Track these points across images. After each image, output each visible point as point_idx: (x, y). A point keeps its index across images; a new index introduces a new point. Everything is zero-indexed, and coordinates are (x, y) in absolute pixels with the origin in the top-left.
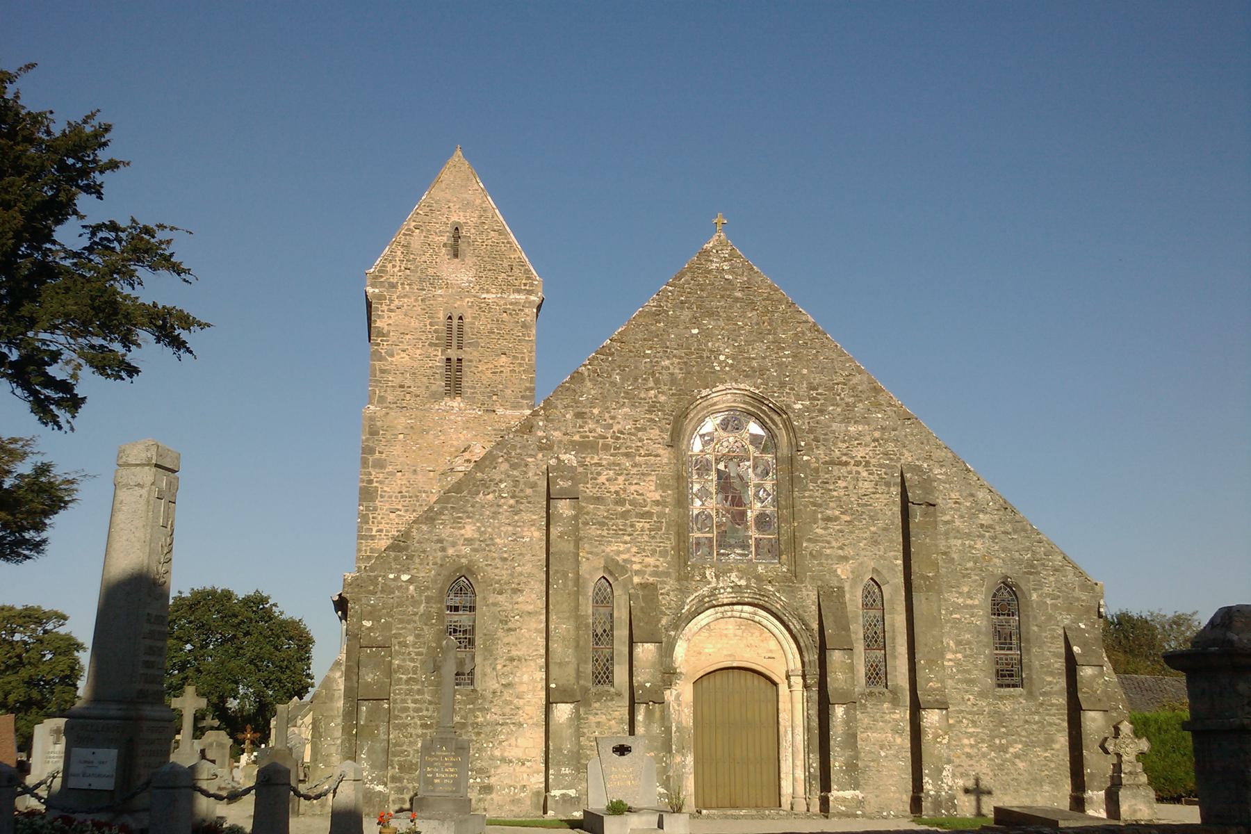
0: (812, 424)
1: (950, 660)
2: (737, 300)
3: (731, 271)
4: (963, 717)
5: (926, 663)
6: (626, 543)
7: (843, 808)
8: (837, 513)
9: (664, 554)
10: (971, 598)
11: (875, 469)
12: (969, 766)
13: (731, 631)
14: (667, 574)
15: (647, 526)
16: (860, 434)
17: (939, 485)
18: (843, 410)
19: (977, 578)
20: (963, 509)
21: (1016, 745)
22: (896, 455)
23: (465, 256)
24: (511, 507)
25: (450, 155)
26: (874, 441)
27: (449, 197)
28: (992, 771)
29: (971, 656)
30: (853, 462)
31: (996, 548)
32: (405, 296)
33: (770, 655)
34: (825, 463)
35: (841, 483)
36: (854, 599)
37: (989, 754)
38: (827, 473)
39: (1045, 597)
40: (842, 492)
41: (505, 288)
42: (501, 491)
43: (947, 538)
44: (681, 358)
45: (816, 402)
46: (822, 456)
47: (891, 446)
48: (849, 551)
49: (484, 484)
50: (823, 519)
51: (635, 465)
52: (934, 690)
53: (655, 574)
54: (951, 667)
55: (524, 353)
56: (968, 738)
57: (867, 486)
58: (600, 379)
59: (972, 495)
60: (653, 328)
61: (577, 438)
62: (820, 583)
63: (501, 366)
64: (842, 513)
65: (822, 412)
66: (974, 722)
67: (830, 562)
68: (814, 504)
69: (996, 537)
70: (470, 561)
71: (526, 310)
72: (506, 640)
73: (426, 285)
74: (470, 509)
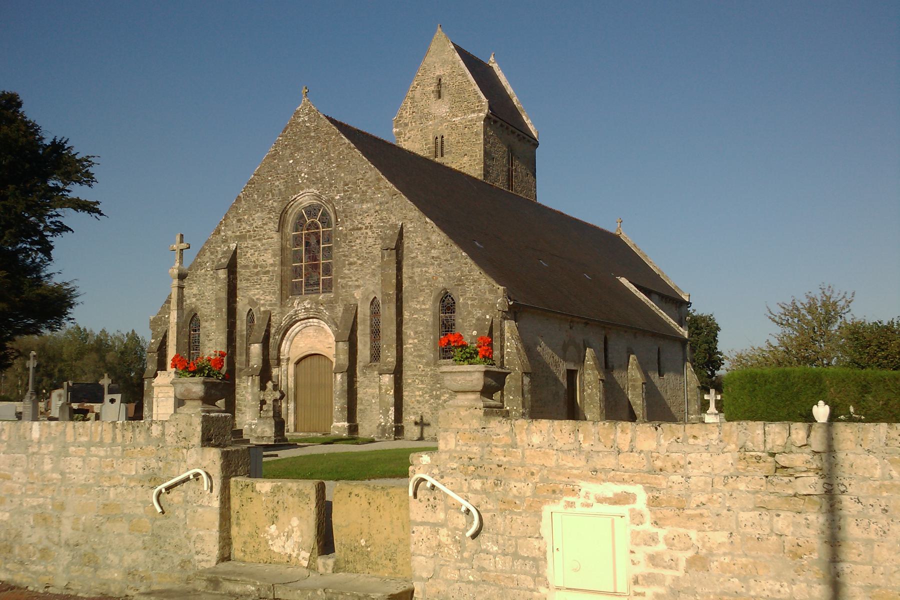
0: (344, 207)
1: (411, 344)
2: (311, 138)
3: (309, 121)
4: (416, 379)
5: (386, 347)
6: (257, 289)
7: (337, 432)
8: (355, 259)
9: (274, 293)
10: (424, 304)
11: (375, 230)
12: (419, 408)
13: (312, 334)
14: (275, 304)
15: (267, 278)
16: (369, 209)
17: (410, 235)
18: (361, 196)
19: (428, 291)
20: (423, 248)
21: (445, 395)
22: (386, 219)
23: (444, 96)
24: (211, 275)
25: (435, 31)
26: (376, 212)
27: (434, 60)
28: (431, 411)
29: (423, 341)
30: (364, 227)
31: (441, 271)
32: (412, 130)
33: (329, 346)
34: (350, 230)
35: (358, 241)
36: (364, 311)
37: (429, 401)
38: (351, 236)
39: (467, 300)
40: (358, 246)
41: (466, 111)
42: (207, 267)
43: (413, 268)
44: (284, 179)
45: (346, 193)
46: (349, 226)
47: (384, 214)
48: (361, 282)
49: (200, 264)
50: (348, 264)
51: (263, 245)
52: (390, 363)
53: (270, 305)
54: (411, 348)
55: (476, 152)
56: (419, 391)
57: (370, 241)
58: (248, 199)
59: (428, 238)
60: (273, 164)
61: (238, 234)
62: (345, 302)
63: (464, 163)
64: (358, 259)
65: (349, 199)
66: (422, 381)
67: (351, 289)
68: (344, 256)
69: (441, 264)
70: (196, 306)
71: (478, 124)
72: (209, 346)
73: (424, 120)
74: (195, 279)
